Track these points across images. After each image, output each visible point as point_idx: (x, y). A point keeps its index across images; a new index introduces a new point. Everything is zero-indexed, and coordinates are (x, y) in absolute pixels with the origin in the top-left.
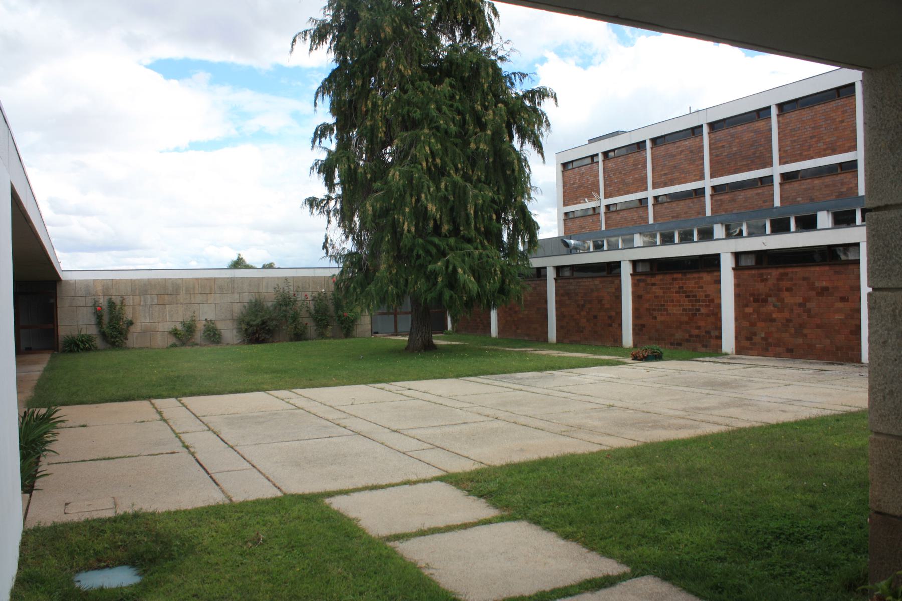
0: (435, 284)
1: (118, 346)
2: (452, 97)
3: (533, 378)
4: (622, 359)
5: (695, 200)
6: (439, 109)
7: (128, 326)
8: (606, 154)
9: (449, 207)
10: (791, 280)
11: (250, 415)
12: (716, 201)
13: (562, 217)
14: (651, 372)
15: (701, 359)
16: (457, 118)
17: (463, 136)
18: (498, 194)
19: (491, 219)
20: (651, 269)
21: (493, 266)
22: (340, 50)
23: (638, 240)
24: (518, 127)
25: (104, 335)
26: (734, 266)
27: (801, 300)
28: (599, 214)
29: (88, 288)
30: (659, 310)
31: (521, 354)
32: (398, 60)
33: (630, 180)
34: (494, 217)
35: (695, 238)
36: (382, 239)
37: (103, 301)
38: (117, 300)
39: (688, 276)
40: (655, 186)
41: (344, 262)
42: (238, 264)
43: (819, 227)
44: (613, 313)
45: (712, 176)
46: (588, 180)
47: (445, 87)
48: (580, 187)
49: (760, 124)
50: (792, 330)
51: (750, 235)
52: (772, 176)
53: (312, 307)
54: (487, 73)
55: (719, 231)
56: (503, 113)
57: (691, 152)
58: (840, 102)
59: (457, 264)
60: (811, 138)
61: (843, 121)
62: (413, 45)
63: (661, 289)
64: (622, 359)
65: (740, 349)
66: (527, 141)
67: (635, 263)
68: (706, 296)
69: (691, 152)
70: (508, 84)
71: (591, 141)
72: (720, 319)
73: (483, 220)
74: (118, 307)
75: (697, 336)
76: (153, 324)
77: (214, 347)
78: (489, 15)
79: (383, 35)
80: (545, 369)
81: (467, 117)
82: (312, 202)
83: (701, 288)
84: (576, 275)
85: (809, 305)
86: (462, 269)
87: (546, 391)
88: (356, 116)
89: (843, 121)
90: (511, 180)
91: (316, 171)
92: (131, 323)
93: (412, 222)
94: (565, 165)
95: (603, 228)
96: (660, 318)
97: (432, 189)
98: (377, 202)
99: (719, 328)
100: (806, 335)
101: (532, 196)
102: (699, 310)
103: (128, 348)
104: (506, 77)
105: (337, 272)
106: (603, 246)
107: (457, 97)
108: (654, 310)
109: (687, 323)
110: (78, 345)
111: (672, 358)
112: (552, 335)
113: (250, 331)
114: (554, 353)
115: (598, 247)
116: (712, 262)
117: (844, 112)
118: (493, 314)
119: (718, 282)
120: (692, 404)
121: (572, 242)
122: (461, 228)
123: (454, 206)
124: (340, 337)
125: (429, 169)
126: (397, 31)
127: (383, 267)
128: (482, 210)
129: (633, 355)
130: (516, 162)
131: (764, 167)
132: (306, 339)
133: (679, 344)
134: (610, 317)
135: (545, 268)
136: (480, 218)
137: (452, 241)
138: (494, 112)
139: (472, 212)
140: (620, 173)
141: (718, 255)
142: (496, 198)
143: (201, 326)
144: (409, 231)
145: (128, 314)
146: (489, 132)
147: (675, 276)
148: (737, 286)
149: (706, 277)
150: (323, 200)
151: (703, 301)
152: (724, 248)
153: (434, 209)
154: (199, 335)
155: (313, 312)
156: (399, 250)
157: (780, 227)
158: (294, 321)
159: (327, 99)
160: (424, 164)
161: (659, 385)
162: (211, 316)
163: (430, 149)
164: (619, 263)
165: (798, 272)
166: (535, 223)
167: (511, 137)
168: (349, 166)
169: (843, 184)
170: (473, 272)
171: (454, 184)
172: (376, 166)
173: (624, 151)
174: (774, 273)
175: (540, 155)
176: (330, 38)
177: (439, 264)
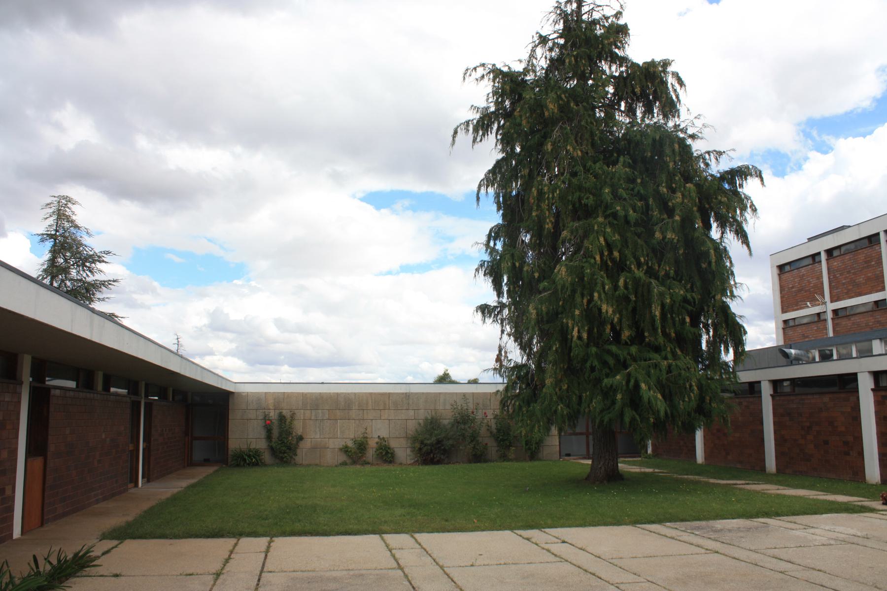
0: (614, 403)
1: (286, 462)
2: (633, 181)
4: (867, 503)
6: (614, 194)
7: (298, 442)
8: (829, 252)
9: (630, 308)
11: (328, 574)
13: (781, 325)
16: (639, 204)
17: (646, 224)
18: (693, 291)
19: (683, 322)
21: (688, 379)
22: (506, 141)
24: (715, 214)
25: (272, 450)
28: (825, 320)
29: (259, 401)
31: (727, 488)
32: (566, 141)
33: (861, 279)
34: (688, 320)
36: (550, 348)
37: (273, 415)
38: (286, 413)
41: (509, 377)
42: (444, 379)
46: (809, 282)
47: (620, 169)
48: (800, 291)
53: (494, 426)
54: (673, 150)
56: (694, 194)
59: (640, 377)
62: (583, 123)
64: (867, 503)
70: (702, 165)
71: (810, 239)
73: (674, 324)
74: (288, 420)
76: (325, 439)
77: (386, 467)
78: (673, 86)
79: (546, 114)
80: (757, 515)
81: (651, 201)
82: (485, 310)
84: (797, 390)
86: (647, 383)
87: (754, 557)
88: (524, 210)
90: (709, 277)
91: (481, 273)
92: (301, 438)
93: (583, 327)
94: (781, 267)
95: (831, 334)
97: (607, 287)
98: (542, 304)
101: (735, 293)
103: (296, 465)
104: (699, 157)
105: (501, 388)
106: (832, 355)
107: (639, 181)
110: (248, 460)
113: (425, 449)
114: (772, 489)
115: (826, 357)
118: (699, 435)
122: (646, 334)
123: (635, 305)
124: (525, 460)
125: (604, 263)
126: (564, 109)
127: (548, 381)
128: (672, 313)
130: (712, 252)
132: (486, 461)
135: (759, 382)
136: (670, 321)
137: (634, 349)
138: (683, 195)
139: (657, 313)
140: (849, 272)
143: (372, 444)
144: (580, 338)
145: (298, 428)
146: (677, 218)
150: (496, 307)
152: (863, 368)
153: (610, 311)
154: (370, 454)
155: (495, 431)
156: (570, 360)
158: (472, 441)
159: (491, 190)
160: (598, 258)
162: (384, 434)
163: (605, 240)
166: (741, 327)
167: (709, 227)
168: (514, 264)
170: (661, 387)
171: (637, 281)
172: (545, 264)
173: (852, 246)
175: (745, 246)
176: (495, 126)
177: (618, 377)
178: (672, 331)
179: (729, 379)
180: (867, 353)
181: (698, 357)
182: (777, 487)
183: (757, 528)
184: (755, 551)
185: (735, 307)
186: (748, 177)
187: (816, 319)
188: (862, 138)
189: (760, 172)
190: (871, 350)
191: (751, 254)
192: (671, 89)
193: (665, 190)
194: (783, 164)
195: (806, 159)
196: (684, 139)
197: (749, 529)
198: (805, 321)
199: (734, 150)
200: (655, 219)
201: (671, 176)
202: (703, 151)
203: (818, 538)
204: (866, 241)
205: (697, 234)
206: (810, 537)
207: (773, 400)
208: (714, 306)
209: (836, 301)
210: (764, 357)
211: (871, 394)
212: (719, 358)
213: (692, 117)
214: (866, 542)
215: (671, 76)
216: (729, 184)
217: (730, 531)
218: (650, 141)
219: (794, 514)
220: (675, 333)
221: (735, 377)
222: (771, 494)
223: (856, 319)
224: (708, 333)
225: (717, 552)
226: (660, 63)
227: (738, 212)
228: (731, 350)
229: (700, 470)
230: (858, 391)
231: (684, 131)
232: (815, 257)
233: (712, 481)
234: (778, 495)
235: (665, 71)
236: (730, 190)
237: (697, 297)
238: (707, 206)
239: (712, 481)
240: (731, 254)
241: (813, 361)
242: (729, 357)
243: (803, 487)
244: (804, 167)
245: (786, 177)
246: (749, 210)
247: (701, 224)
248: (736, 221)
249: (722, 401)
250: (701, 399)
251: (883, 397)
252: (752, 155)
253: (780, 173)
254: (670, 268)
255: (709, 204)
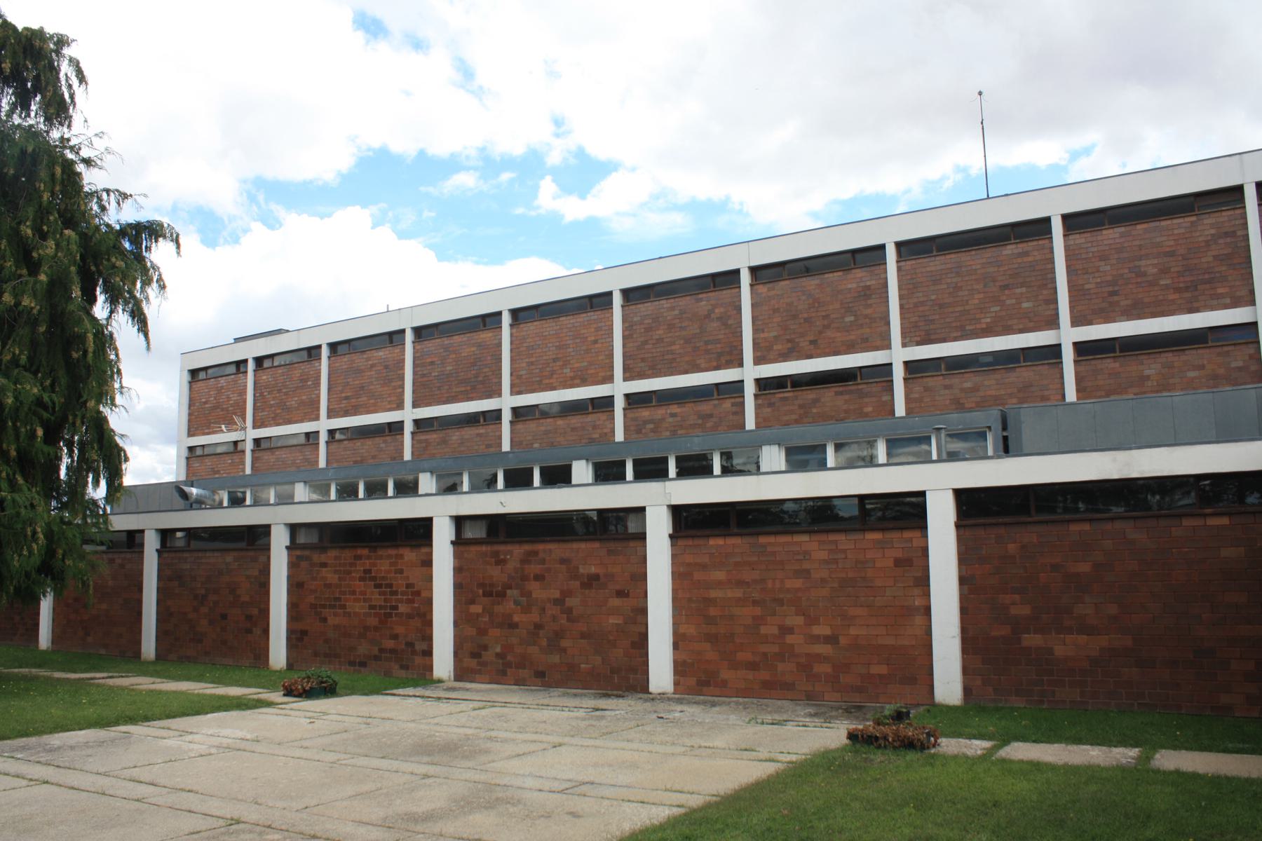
3: (87, 745)
5: (388, 438)
8: (259, 361)
10: (543, 562)
12: (420, 442)
13: (185, 453)
14: (318, 723)
15: (400, 691)
19: (33, 435)
20: (321, 539)
21: (31, 522)
23: (301, 492)
26: (453, 538)
27: (557, 595)
28: (243, 452)
30: (333, 607)
33: (293, 402)
34: (40, 432)
35: (391, 492)
39: (381, 552)
40: (331, 414)
43: (574, 482)
44: (255, 612)
45: (415, 405)
46: (229, 398)
48: (215, 408)
49: (485, 336)
50: (544, 643)
51: (475, 489)
52: (500, 410)
54: (53, 175)
55: (427, 483)
56: (74, 247)
57: (386, 367)
58: (593, 316)
60: (554, 360)
61: (595, 342)
63: (335, 572)
65: (462, 673)
66: (120, 308)
67: (294, 528)
68: (408, 586)
69: (386, 367)
70: (95, 207)
71: (237, 340)
72: (429, 623)
75: (392, 651)
80: (117, 723)
83: (401, 572)
84: (195, 544)
85: (570, 602)
89: (595, 342)
90: (85, 372)
94: (194, 373)
95: (248, 471)
96: (332, 621)
99: (428, 638)
100: (564, 650)
102: (396, 608)
106: (244, 500)
108: (324, 606)
109: (376, 629)
111: (352, 691)
112: (149, 647)
114: (145, 683)
115: (237, 501)
116: (420, 530)
117: (598, 329)
118: (46, 606)
119: (428, 563)
120: (401, 806)
121: (194, 491)
129: (285, 688)
130: (90, 336)
131: (489, 396)
133: (363, 664)
134: (249, 617)
135: (142, 531)
138: (57, 245)
140: (279, 391)
141: (430, 520)
142: (46, 398)
147: (360, 552)
148: (458, 570)
149: (409, 555)
151: (403, 593)
152: (439, 509)
157: (518, 480)
161: (331, 757)
164: (268, 527)
165: (554, 550)
166: (121, 449)
167: (93, 300)
169: (595, 427)
173: (288, 359)
174: (516, 551)
175: (141, 336)
178: (13, 447)
179: (96, 525)
180: (286, 500)
181: (52, 490)
182: (152, 680)
183: (113, 741)
184: (105, 775)
185: (116, 420)
186: (161, 239)
187: (231, 448)
188: (318, 219)
189: (178, 236)
190: (292, 496)
191: (148, 348)
192: (63, 82)
193: (29, 232)
194: (215, 229)
195: (246, 231)
196: (72, 162)
197: (101, 743)
198: (220, 450)
199: (145, 196)
200: (6, 272)
201: (42, 213)
202: (100, 187)
203: (195, 746)
204: (305, 353)
205: (71, 307)
206: (185, 746)
207: (159, 556)
208: (83, 417)
209: (259, 427)
210: (152, 496)
211: (285, 553)
212: (84, 494)
213: (90, 133)
214: (258, 748)
215: (66, 62)
216: (131, 243)
217: (72, 748)
218: (16, 151)
219: (169, 717)
220: (18, 451)
221: (106, 522)
222: (141, 691)
223: (282, 454)
224: (71, 454)
225: (47, 782)
226: (52, 37)
227: (139, 285)
228: (103, 483)
229: (44, 660)
230: (269, 549)
231: (75, 150)
232: (240, 364)
233: (57, 675)
234: (152, 691)
235: (58, 52)
236: (131, 252)
237: (58, 399)
238: (93, 268)
239: (57, 675)
240: (118, 344)
241: (220, 506)
242: (98, 492)
243: (188, 679)
244: (242, 240)
245: (218, 248)
246: (155, 285)
247: (79, 293)
248: (134, 297)
249: (82, 556)
250: (50, 552)
251: (298, 557)
252: (175, 209)
253: (210, 241)
254: (21, 352)
255: (97, 265)
